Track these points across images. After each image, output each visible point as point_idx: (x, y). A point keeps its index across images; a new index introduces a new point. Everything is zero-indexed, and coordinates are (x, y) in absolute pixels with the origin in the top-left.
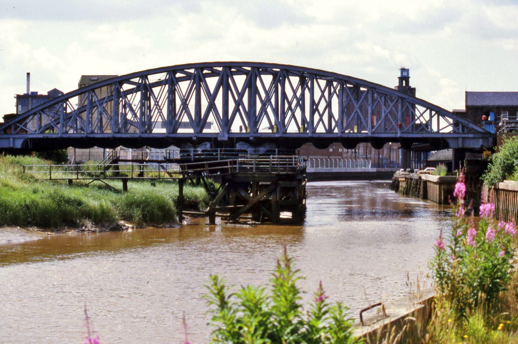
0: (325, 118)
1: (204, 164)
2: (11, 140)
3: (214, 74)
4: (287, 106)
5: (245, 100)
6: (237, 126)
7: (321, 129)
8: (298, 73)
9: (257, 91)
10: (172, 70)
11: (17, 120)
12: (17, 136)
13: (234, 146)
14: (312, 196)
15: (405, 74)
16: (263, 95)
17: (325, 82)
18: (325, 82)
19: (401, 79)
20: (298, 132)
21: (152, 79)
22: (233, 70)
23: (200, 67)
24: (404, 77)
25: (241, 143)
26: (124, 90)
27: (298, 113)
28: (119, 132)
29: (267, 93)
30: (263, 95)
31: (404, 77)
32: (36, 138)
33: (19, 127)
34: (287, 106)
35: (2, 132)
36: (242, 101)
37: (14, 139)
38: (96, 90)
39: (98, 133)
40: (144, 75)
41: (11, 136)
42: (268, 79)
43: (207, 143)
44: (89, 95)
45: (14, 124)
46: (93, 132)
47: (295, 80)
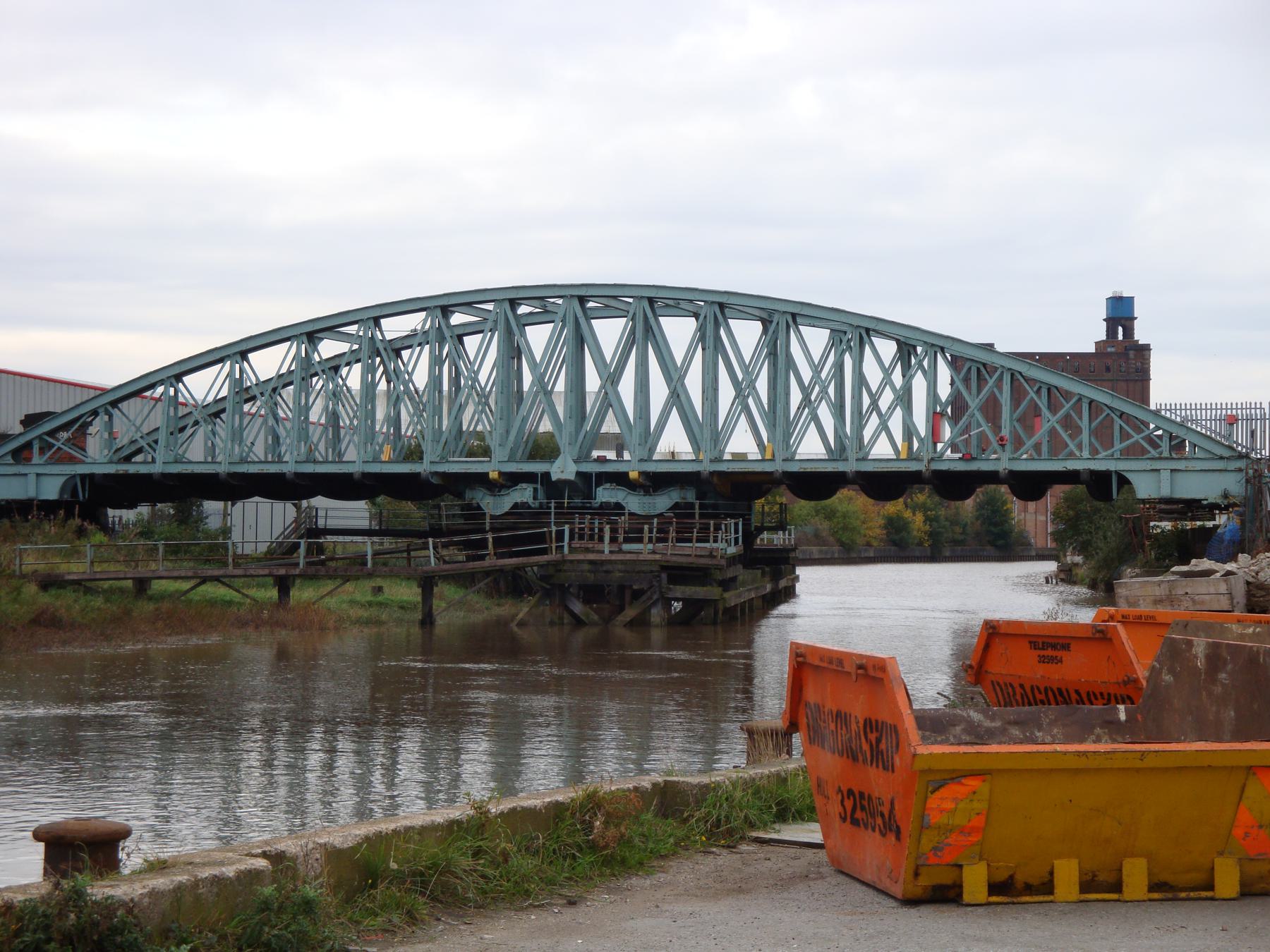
1: (563, 541)
2: (32, 478)
3: (544, 316)
4: (866, 401)
5: (762, 385)
6: (743, 443)
7: (882, 450)
8: (757, 312)
9: (790, 363)
10: (443, 307)
11: (47, 427)
13: (590, 495)
17: (690, 324)
18: (690, 324)
20: (760, 457)
21: (394, 328)
22: (591, 304)
23: (512, 298)
25: (608, 485)
26: (324, 357)
28: (376, 460)
33: (53, 445)
34: (866, 401)
35: (9, 459)
36: (754, 388)
37: (38, 475)
38: (250, 356)
39: (326, 462)
40: (374, 316)
43: (524, 485)
44: (232, 368)
45: (40, 437)
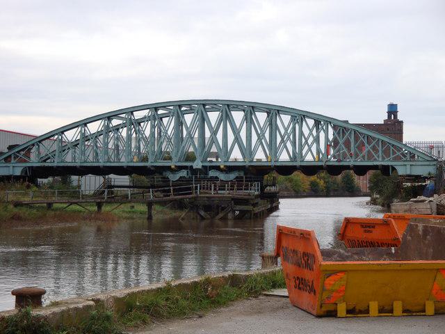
0: (314, 149)
2: (11, 167)
3: (191, 111)
4: (304, 141)
6: (260, 156)
9: (277, 128)
11: (17, 150)
12: (16, 165)
14: (239, 297)
15: (393, 110)
16: (283, 131)
19: (390, 113)
21: (138, 115)
23: (179, 105)
24: (393, 110)
27: (289, 145)
29: (286, 130)
30: (283, 131)
31: (393, 110)
32: (67, 167)
34: (304, 141)
39: (114, 162)
40: (131, 111)
41: (11, 165)
42: (286, 119)
46: (329, 161)
47: (311, 122)
